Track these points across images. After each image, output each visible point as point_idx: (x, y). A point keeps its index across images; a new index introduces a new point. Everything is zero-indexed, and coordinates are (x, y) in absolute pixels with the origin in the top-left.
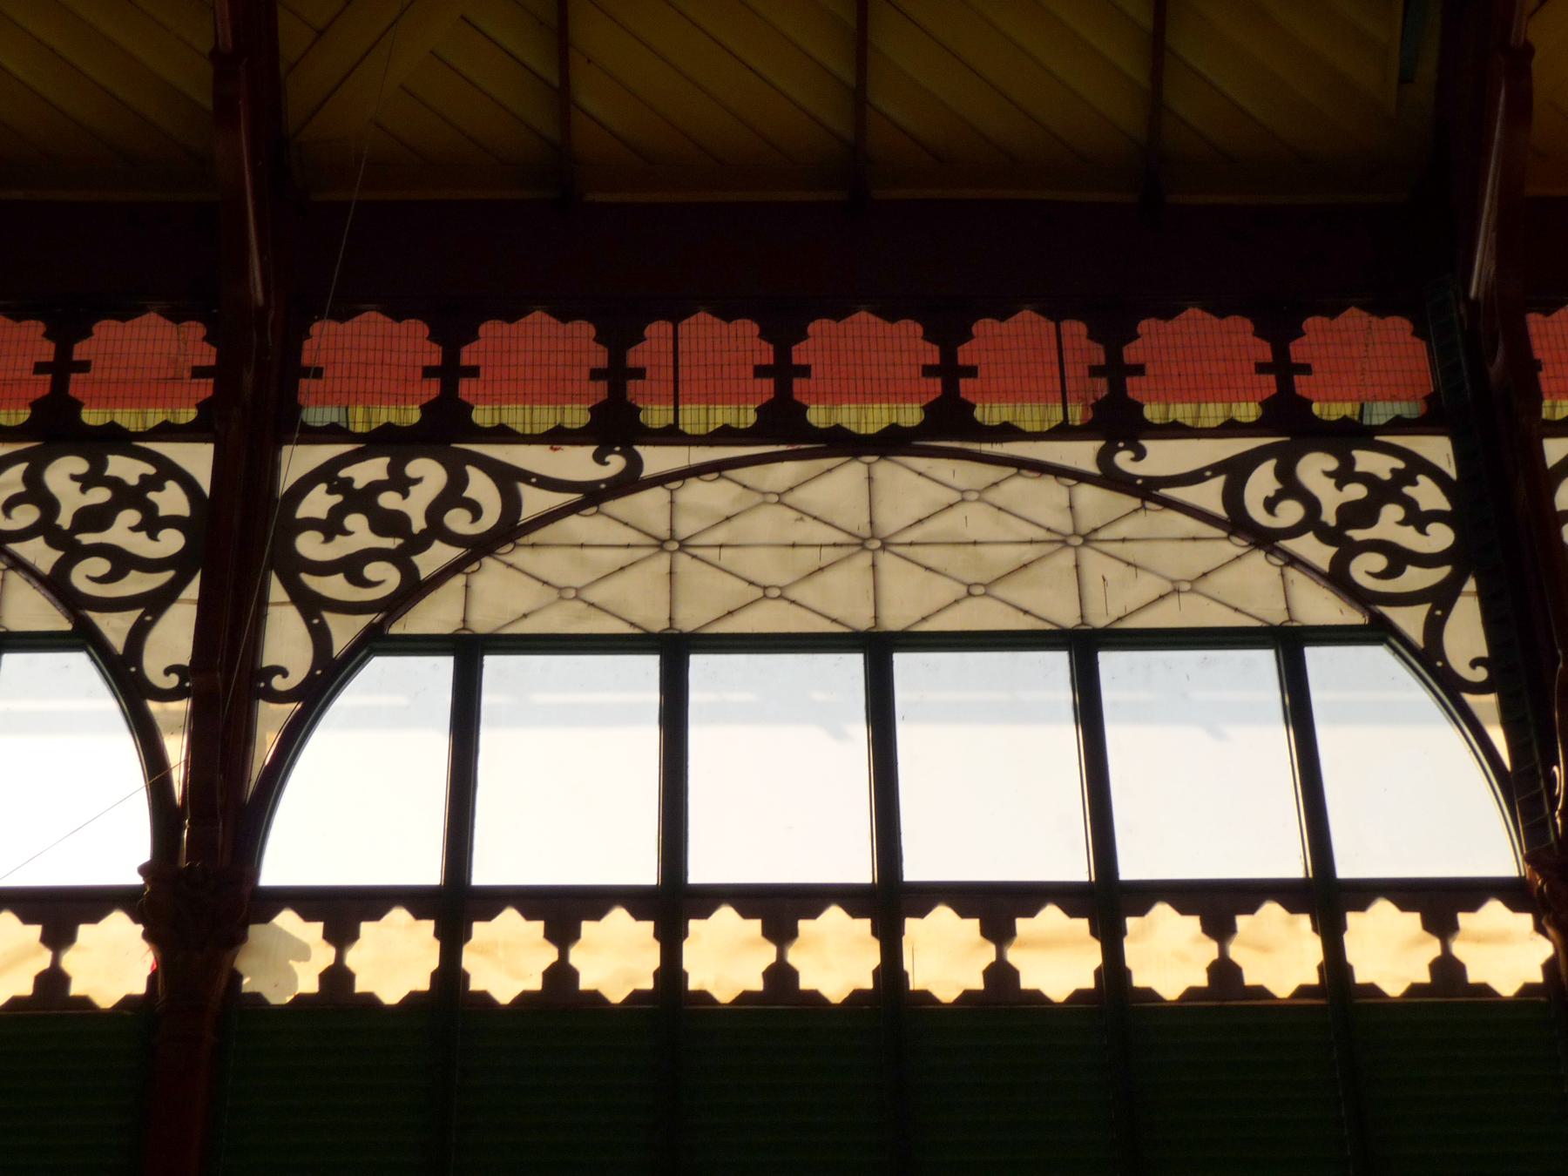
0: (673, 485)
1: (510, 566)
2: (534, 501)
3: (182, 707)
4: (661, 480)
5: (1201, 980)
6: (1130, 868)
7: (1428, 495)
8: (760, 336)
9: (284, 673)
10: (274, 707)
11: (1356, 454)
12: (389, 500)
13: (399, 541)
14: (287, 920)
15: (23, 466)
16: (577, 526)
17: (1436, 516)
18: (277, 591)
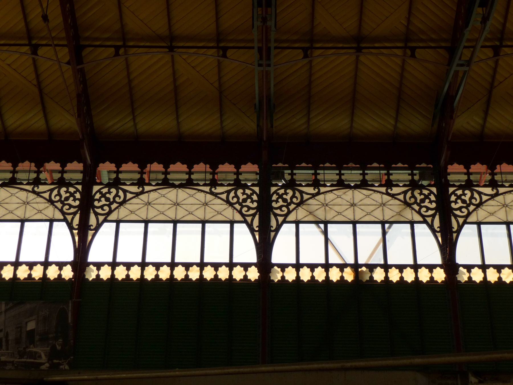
0: (504, 195)
1: (125, 207)
2: (484, 198)
3: (77, 231)
4: (502, 194)
5: (429, 279)
6: (302, 261)
7: (433, 198)
8: (234, 168)
9: (92, 226)
10: (91, 231)
11: (246, 190)
12: (108, 195)
13: (109, 203)
14: (91, 266)
15: (234, 191)
16: (491, 202)
17: (433, 201)
18: (92, 211)
